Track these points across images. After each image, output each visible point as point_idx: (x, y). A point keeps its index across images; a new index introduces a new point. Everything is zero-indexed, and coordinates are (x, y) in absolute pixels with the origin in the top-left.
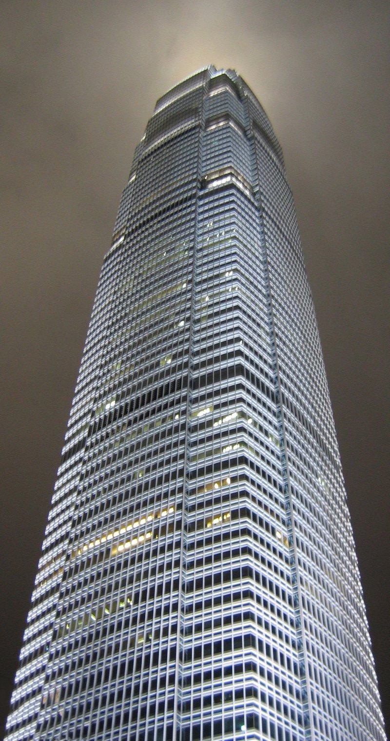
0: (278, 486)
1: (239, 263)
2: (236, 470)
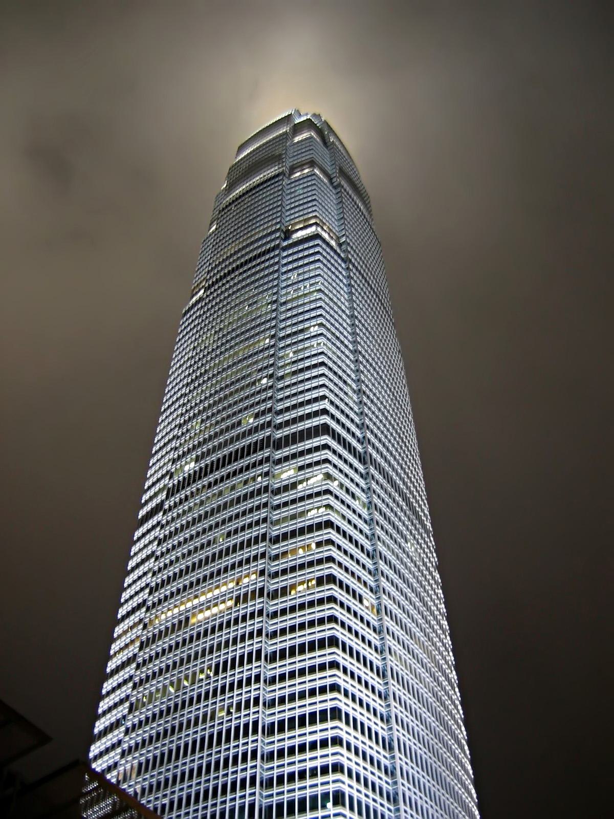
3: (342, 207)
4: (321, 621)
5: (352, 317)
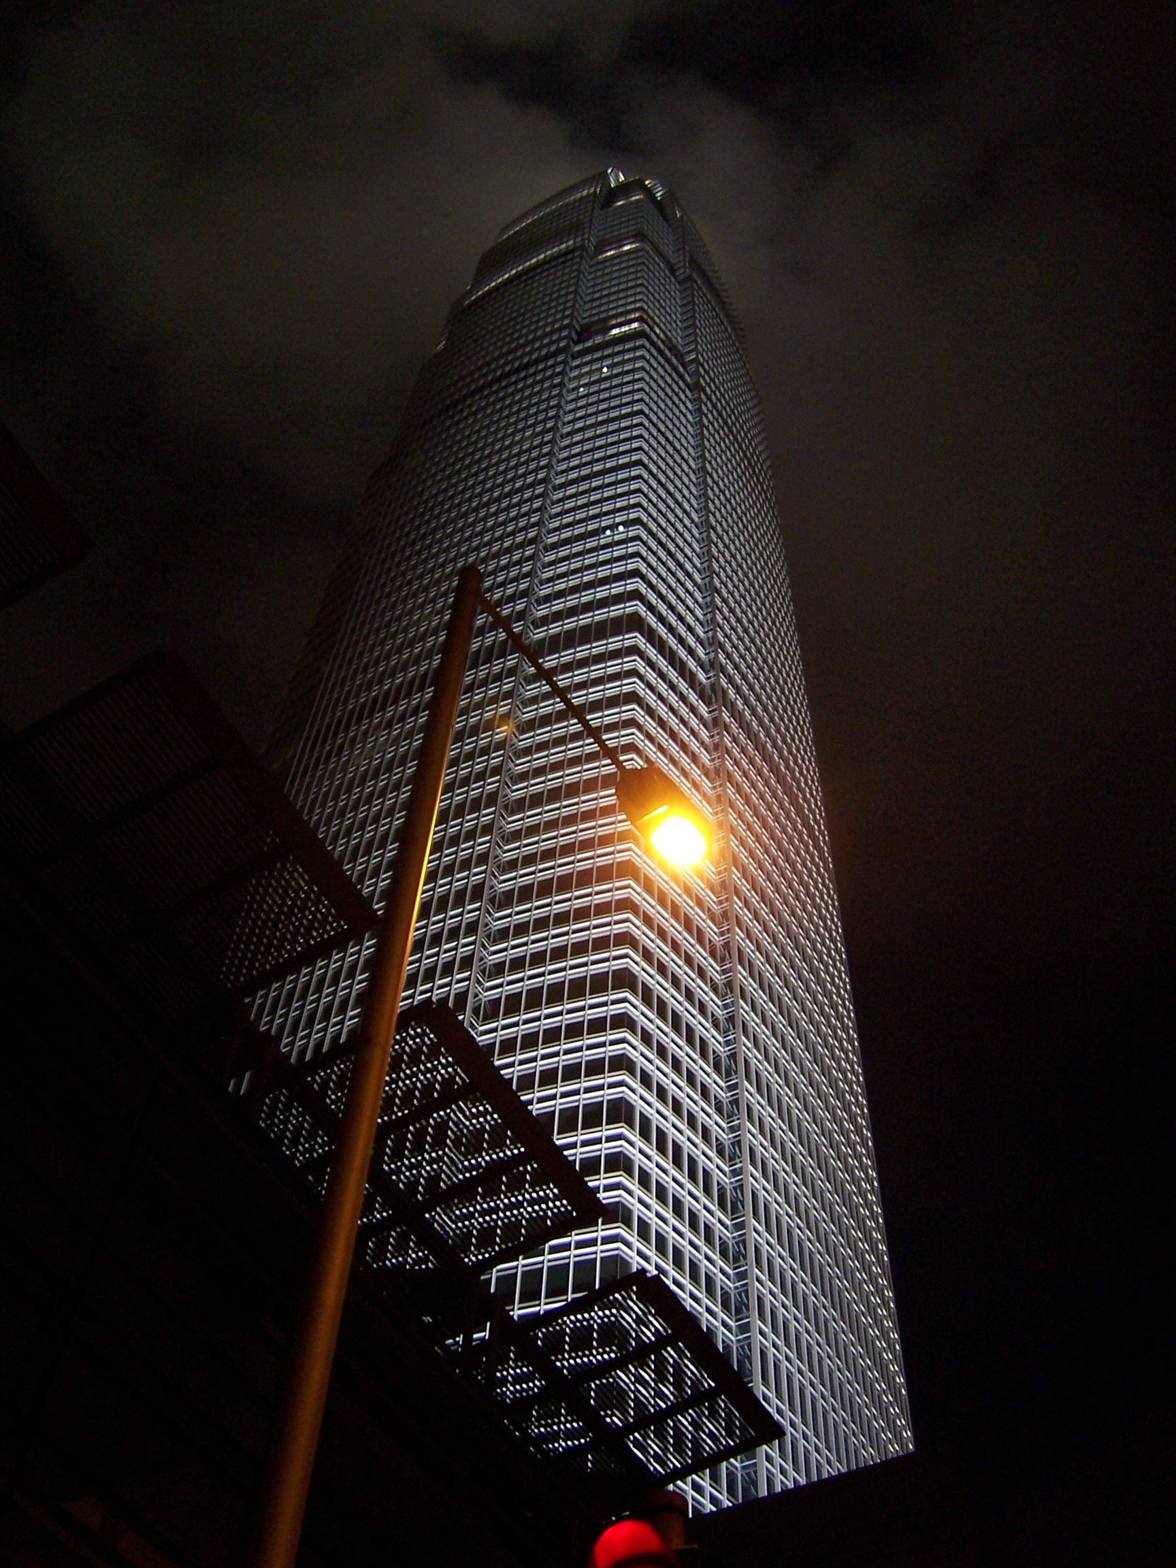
0: (711, 1057)
1: (643, 578)
2: (605, 1004)
3: (694, 325)
4: (595, 1068)
5: (710, 645)
